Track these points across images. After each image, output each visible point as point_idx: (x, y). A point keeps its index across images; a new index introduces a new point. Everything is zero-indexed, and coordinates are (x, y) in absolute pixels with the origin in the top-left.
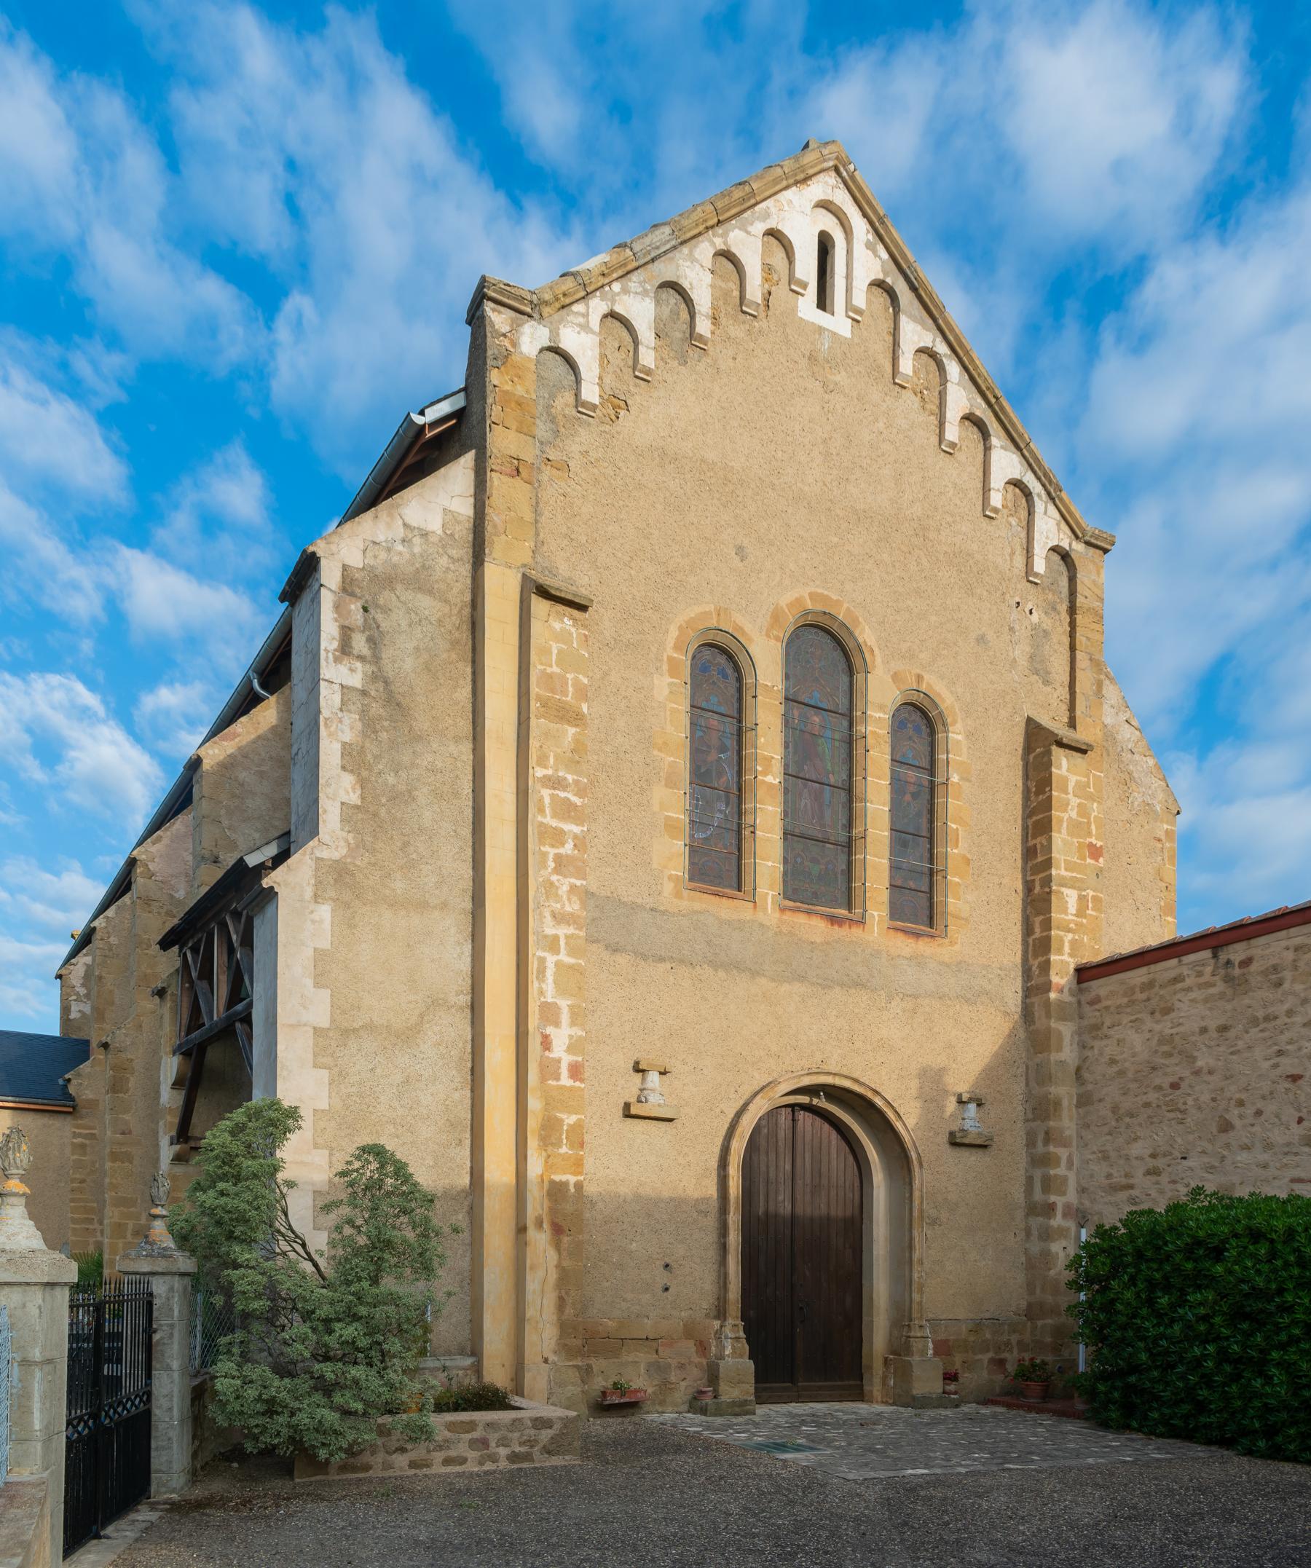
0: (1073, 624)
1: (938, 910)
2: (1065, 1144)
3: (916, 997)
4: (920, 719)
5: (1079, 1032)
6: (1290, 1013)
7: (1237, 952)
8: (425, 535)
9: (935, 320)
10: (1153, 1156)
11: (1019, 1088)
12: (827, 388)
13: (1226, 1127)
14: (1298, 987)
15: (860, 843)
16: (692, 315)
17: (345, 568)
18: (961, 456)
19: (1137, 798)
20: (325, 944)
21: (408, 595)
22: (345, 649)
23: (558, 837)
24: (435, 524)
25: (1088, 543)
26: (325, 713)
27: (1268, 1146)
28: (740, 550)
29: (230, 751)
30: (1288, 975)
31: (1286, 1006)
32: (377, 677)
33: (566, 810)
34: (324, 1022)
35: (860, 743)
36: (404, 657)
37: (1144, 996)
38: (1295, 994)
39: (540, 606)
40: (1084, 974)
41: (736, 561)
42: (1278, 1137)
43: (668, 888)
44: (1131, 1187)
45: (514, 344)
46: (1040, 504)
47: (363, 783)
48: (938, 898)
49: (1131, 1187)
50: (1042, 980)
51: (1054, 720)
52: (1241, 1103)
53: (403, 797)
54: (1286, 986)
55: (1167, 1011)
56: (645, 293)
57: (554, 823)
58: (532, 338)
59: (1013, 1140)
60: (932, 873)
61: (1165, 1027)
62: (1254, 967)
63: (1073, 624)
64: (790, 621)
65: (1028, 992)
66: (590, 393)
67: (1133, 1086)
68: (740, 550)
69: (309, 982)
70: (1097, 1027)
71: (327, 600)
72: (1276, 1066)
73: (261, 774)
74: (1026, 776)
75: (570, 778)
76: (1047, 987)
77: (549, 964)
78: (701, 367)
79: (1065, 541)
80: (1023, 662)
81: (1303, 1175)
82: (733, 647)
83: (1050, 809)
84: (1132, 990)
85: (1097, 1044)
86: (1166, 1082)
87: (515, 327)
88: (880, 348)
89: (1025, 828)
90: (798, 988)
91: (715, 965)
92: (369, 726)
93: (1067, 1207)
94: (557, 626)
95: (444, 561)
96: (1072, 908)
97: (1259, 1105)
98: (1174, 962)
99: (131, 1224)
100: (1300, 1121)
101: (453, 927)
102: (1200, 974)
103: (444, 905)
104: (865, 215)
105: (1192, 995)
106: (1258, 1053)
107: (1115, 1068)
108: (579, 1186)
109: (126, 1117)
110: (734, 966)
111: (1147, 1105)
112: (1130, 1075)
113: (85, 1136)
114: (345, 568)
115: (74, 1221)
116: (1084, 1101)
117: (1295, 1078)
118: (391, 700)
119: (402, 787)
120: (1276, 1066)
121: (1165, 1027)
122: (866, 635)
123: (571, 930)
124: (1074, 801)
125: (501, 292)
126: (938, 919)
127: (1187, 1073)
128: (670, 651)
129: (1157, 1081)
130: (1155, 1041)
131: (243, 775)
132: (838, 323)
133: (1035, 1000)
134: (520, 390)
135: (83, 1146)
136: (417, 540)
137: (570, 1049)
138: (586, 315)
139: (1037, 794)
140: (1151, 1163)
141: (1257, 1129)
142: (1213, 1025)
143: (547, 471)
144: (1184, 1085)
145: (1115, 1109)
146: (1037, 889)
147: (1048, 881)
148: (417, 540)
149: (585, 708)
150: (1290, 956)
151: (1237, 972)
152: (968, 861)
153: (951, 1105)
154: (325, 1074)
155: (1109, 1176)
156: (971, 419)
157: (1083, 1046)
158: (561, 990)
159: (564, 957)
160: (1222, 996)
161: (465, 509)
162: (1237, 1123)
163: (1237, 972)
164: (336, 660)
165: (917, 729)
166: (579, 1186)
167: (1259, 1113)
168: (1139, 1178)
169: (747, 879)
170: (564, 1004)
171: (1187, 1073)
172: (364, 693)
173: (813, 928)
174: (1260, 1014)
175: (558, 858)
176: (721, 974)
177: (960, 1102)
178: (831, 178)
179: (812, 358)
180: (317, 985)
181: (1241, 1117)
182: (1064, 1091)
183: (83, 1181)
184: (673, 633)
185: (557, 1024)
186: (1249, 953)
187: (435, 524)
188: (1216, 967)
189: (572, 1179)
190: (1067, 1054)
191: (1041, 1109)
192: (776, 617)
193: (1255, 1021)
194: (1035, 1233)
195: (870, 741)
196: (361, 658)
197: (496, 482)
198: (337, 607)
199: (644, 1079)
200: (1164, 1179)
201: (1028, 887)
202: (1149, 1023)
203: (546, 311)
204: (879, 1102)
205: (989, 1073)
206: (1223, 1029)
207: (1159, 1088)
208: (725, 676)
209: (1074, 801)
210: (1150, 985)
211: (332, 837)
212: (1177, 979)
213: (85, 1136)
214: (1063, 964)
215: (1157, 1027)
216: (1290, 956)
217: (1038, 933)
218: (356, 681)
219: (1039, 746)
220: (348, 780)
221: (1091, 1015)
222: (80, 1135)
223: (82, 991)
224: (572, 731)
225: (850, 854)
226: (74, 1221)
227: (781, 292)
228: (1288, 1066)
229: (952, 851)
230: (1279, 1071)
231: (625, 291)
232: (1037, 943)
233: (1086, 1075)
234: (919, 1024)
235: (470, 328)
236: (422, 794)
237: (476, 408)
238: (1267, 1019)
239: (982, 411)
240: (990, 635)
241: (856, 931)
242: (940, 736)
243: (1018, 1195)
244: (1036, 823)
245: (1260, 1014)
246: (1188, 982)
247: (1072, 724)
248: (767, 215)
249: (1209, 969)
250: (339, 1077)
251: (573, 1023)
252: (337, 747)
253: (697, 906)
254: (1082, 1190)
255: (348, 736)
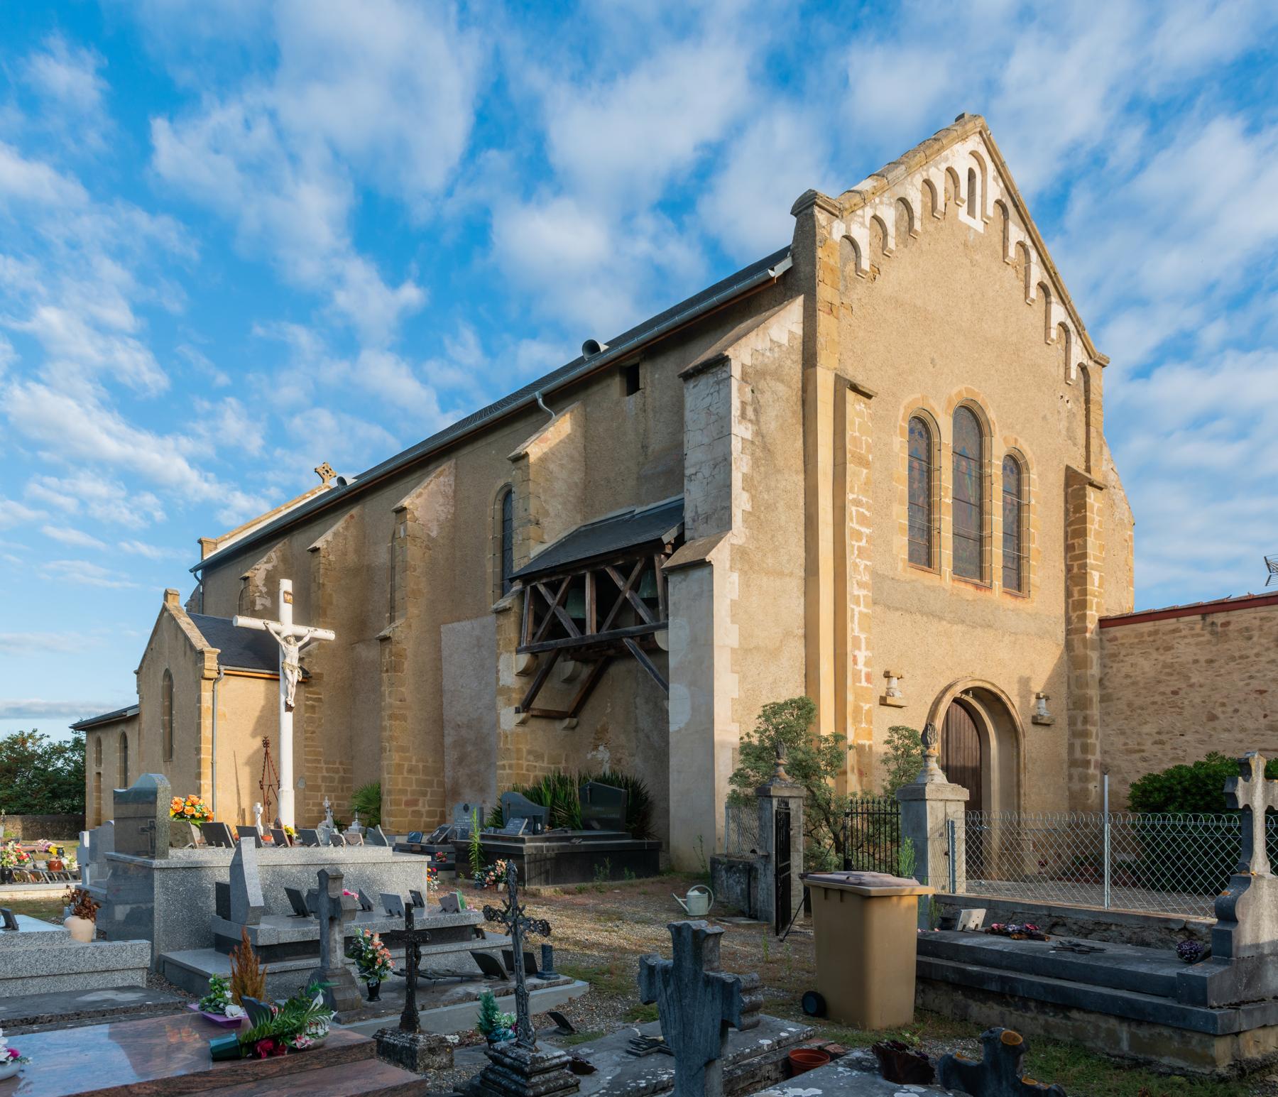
0: (1088, 410)
1: (1024, 581)
2: (1094, 724)
3: (1016, 634)
4: (1015, 465)
5: (1101, 657)
6: (1257, 655)
7: (1220, 618)
8: (780, 346)
9: (1026, 225)
10: (1159, 733)
11: (1064, 690)
12: (973, 263)
13: (1213, 718)
14: (1263, 641)
15: (988, 540)
16: (911, 218)
17: (743, 365)
18: (1035, 306)
19: (1117, 516)
20: (735, 597)
21: (772, 383)
22: (743, 415)
23: (859, 535)
24: (784, 340)
25: (1096, 362)
26: (734, 455)
27: (1243, 730)
28: (932, 360)
29: (545, 450)
30: (1256, 633)
31: (1255, 651)
32: (758, 433)
33: (863, 520)
34: (736, 646)
35: (988, 480)
36: (771, 423)
37: (1151, 639)
38: (1262, 645)
39: (850, 395)
40: (1104, 623)
41: (931, 368)
42: (1250, 724)
43: (900, 566)
44: (1143, 751)
45: (830, 233)
46: (1074, 338)
47: (753, 498)
48: (1024, 574)
49: (1143, 751)
50: (1080, 625)
51: (1081, 469)
52: (1223, 705)
53: (771, 507)
54: (1255, 639)
55: (1168, 649)
56: (890, 204)
57: (857, 527)
58: (838, 230)
59: (1062, 721)
60: (1019, 558)
61: (1168, 657)
62: (1231, 627)
63: (1088, 410)
64: (956, 402)
65: (1069, 632)
66: (865, 265)
67: (1143, 691)
68: (932, 360)
69: (728, 620)
70: (1114, 655)
71: (735, 384)
72: (1248, 684)
73: (562, 466)
74: (1066, 502)
75: (864, 500)
76: (1085, 630)
77: (856, 611)
78: (914, 249)
79: (1086, 361)
80: (1064, 432)
81: (1267, 747)
82: (929, 419)
83: (1085, 522)
84: (1142, 635)
85: (1115, 665)
86: (1168, 690)
87: (830, 223)
88: (997, 239)
89: (1066, 533)
90: (960, 628)
91: (922, 613)
92: (756, 463)
93: (1096, 762)
94: (858, 407)
95: (789, 362)
96: (1097, 584)
97: (1237, 706)
98: (1174, 620)
99: (406, 765)
100: (1265, 716)
101: (795, 585)
102: (1192, 629)
103: (791, 574)
104: (993, 160)
105: (1187, 641)
106: (1236, 676)
107: (1129, 681)
108: (870, 747)
109: (403, 689)
110: (932, 614)
111: (1154, 703)
112: (1141, 685)
113: (314, 700)
114: (743, 365)
115: (307, 761)
116: (1105, 699)
117: (1261, 692)
118: (766, 449)
119: (771, 501)
120: (1248, 684)
121: (1168, 657)
122: (991, 414)
123: (865, 592)
124: (1097, 519)
125: (825, 202)
126: (1024, 586)
127: (1184, 686)
128: (900, 422)
129: (1162, 690)
130: (1159, 666)
131: (552, 466)
132: (977, 224)
133: (1075, 637)
134: (832, 262)
135: (313, 707)
136: (776, 349)
137: (866, 664)
138: (863, 217)
139: (1075, 512)
140: (1157, 737)
141: (1235, 720)
142: (1202, 658)
143: (843, 311)
144: (1182, 693)
145: (1130, 705)
146: (1075, 570)
147: (1084, 566)
148: (776, 349)
149: (870, 458)
150: (1257, 622)
151: (1219, 629)
152: (1039, 552)
153: (1033, 700)
154: (736, 676)
155: (1125, 744)
156: (1042, 286)
157: (1104, 666)
158: (862, 629)
159: (862, 609)
160: (1209, 642)
161: (798, 330)
162: (1221, 716)
163: (1219, 629)
164: (740, 422)
165: (1012, 471)
166: (870, 747)
167: (1236, 711)
168: (1148, 746)
169: (936, 560)
170: (863, 636)
171: (1184, 686)
172: (752, 442)
173: (968, 591)
174: (1237, 654)
175: (859, 548)
176: (925, 618)
177: (1038, 698)
178: (977, 138)
179: (965, 245)
180: (733, 622)
181: (1223, 712)
182: (1094, 693)
183: (313, 732)
184: (902, 411)
185: (860, 649)
186: (1227, 619)
187: (784, 340)
188: (1204, 625)
189: (867, 743)
190: (1095, 670)
191: (1078, 704)
192: (950, 401)
193: (1233, 658)
194: (1076, 778)
195: (994, 478)
196: (750, 421)
197: (823, 319)
198: (739, 390)
199: (889, 682)
200: (1168, 747)
201: (1069, 569)
202: (1155, 655)
203: (845, 213)
204: (1003, 696)
205: (1051, 681)
206: (1210, 661)
207: (1164, 693)
208: (921, 436)
209: (1097, 519)
210: (1156, 632)
211: (739, 533)
212: (1174, 631)
213: (314, 700)
214: (1093, 616)
215: (1162, 658)
216: (1257, 622)
217: (1076, 596)
218: (748, 435)
219: (1076, 485)
220: (745, 496)
221: (1110, 648)
222: (311, 699)
223: (264, 590)
224: (865, 471)
225: (981, 546)
226: (307, 761)
227: (951, 204)
228: (1256, 684)
229: (1032, 546)
230: (1250, 688)
231: (881, 203)
232: (1076, 600)
233: (1107, 683)
234: (1018, 652)
235: (795, 219)
236: (781, 505)
237: (804, 269)
238: (1241, 657)
239: (1048, 282)
240: (1049, 416)
241: (988, 593)
242: (1025, 475)
243: (1065, 755)
244: (1074, 531)
245: (1237, 654)
246: (1184, 633)
247: (1088, 469)
248: (947, 159)
249: (1198, 627)
250: (743, 679)
251: (867, 649)
252: (740, 475)
253: (914, 577)
254: (1104, 752)
255: (745, 469)
